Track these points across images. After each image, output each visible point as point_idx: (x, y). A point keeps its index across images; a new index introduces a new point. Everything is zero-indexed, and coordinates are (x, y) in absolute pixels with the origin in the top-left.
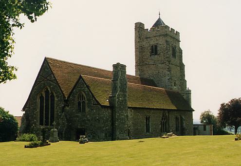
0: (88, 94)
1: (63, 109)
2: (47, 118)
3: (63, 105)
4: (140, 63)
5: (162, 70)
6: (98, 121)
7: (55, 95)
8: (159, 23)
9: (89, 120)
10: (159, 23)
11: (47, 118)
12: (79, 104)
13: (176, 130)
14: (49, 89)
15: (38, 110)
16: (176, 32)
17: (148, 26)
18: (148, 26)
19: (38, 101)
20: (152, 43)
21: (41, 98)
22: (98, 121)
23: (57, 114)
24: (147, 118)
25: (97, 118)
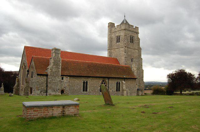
4: (110, 48)
5: (121, 52)
8: (125, 23)
10: (125, 23)
13: (117, 91)
16: (136, 27)
20: (117, 35)
24: (84, 83)
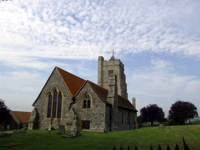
0: (94, 95)
1: (70, 105)
2: (54, 112)
3: (70, 103)
6: (102, 115)
7: (62, 94)
8: (113, 59)
9: (94, 114)
11: (54, 112)
12: (85, 101)
14: (58, 90)
15: (46, 106)
17: (107, 58)
18: (107, 58)
19: (47, 98)
20: (110, 69)
21: (50, 96)
22: (102, 115)
23: (65, 110)
25: (102, 113)
